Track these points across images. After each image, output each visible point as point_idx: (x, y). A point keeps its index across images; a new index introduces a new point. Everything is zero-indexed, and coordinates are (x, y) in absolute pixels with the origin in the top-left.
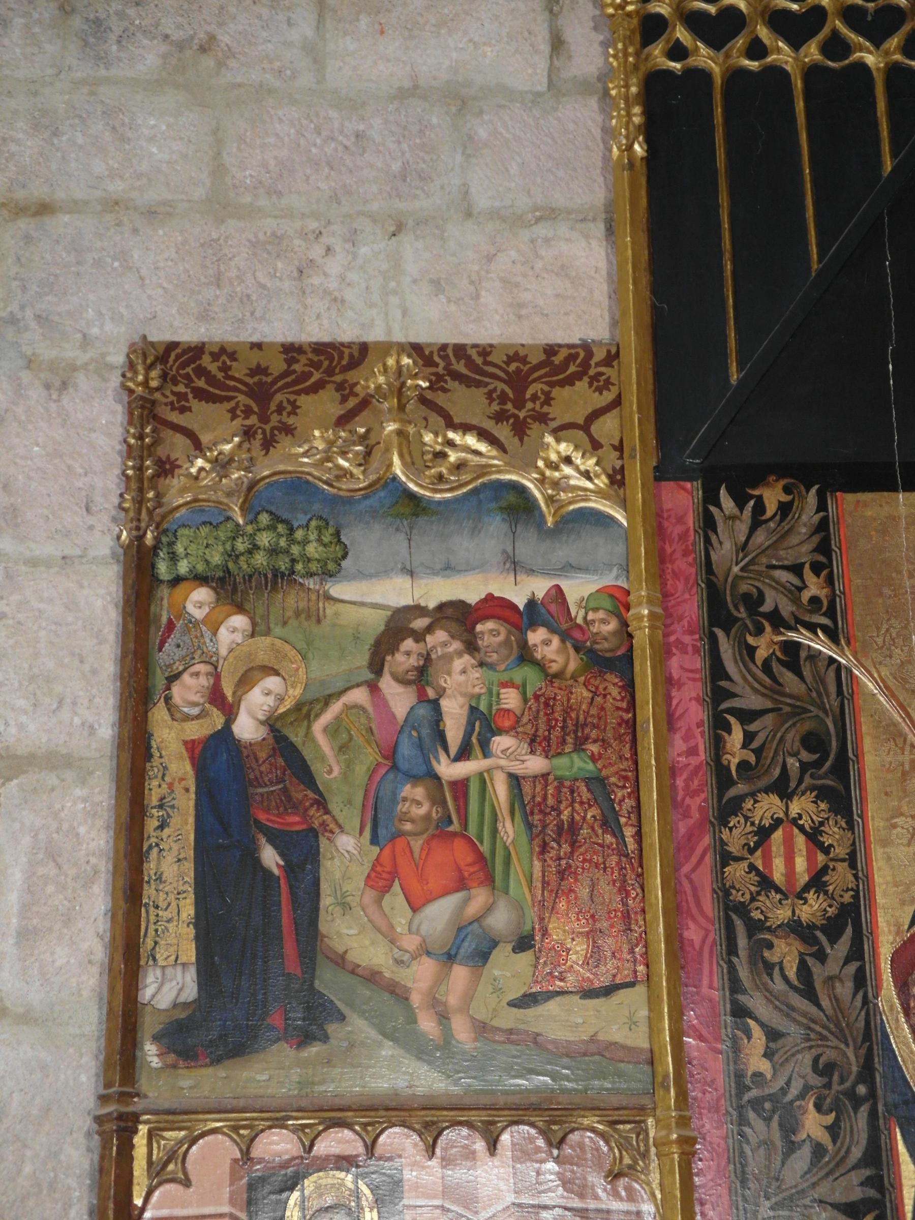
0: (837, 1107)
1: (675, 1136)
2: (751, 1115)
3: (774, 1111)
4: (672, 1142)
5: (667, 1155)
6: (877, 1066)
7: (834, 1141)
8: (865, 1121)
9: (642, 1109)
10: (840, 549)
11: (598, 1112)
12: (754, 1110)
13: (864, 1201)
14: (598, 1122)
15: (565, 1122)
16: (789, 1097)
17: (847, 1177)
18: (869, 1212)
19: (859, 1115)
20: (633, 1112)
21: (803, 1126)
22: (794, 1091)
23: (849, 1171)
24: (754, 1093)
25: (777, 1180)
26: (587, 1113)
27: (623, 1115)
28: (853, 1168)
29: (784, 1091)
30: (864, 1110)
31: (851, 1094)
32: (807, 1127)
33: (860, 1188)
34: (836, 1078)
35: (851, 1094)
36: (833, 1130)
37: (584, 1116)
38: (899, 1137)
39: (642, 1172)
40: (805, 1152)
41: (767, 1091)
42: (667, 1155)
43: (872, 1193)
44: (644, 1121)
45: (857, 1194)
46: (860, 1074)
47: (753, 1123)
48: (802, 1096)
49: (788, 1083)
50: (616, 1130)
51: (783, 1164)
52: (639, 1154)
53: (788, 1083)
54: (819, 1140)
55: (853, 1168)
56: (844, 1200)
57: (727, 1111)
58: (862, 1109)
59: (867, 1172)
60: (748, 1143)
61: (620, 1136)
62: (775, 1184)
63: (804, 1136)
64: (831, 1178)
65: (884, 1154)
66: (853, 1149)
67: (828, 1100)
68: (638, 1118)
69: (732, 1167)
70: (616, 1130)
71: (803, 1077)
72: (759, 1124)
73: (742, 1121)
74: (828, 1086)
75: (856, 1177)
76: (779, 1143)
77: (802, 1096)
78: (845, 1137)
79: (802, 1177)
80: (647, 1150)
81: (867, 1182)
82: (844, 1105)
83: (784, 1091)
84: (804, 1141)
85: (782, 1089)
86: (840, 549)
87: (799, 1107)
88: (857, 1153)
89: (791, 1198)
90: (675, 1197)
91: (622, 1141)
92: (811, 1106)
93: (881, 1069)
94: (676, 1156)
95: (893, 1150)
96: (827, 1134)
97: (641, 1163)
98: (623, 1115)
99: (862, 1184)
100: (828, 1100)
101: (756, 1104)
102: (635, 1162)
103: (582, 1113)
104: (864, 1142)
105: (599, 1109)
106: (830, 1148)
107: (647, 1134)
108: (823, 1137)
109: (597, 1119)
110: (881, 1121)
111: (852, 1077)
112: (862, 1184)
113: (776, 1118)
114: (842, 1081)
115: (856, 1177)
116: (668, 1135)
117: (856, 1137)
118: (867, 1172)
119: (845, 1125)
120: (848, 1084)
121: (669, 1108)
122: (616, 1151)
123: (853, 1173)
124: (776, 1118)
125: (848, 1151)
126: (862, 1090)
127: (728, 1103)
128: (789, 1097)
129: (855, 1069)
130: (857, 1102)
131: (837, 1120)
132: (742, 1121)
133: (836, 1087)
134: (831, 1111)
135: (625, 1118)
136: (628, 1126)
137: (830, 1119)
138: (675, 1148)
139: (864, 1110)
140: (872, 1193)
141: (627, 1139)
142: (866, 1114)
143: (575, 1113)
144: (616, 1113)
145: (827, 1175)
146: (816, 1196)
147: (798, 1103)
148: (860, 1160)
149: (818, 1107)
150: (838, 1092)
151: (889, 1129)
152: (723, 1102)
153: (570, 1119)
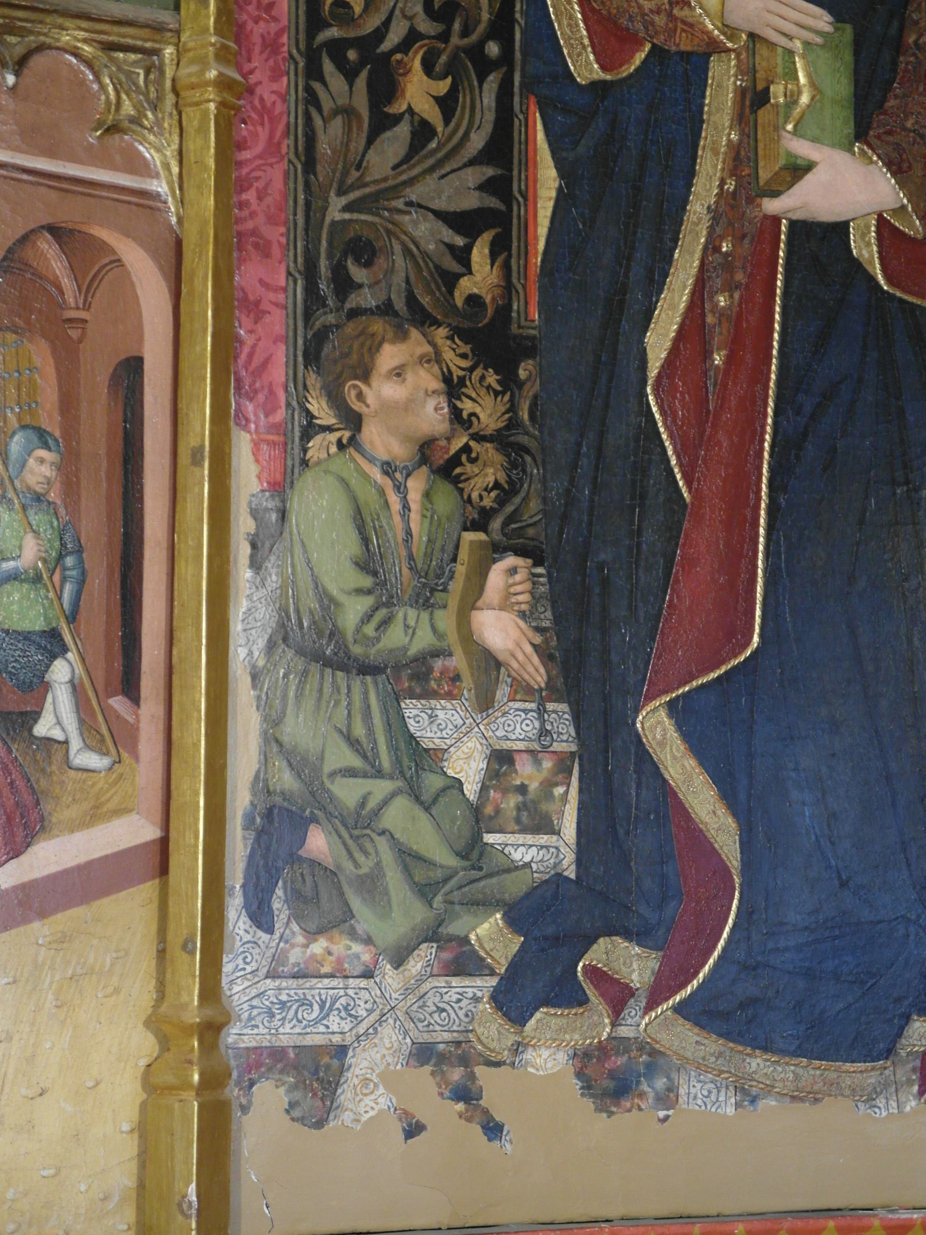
0: (451, 70)
1: (212, 74)
2: (328, 66)
3: (362, 64)
4: (207, 83)
5: (197, 104)
6: (518, 16)
7: (447, 121)
8: (493, 96)
9: (158, 29)
10: (524, 287)
11: (84, 24)
12: (333, 59)
13: (480, 213)
14: (85, 41)
15: (31, 32)
16: (386, 46)
17: (462, 173)
18: (487, 228)
19: (486, 86)
20: (145, 33)
21: (403, 92)
22: (394, 38)
23: (465, 166)
24: (333, 32)
25: (359, 167)
26: (68, 23)
27: (127, 36)
28: (471, 163)
29: (380, 34)
30: (492, 81)
31: (476, 53)
32: (408, 95)
33: (477, 194)
34: (457, 26)
35: (476, 53)
36: (447, 104)
37: (62, 28)
38: (541, 136)
39: (150, 130)
40: (403, 130)
41: (352, 34)
42: (197, 104)
43: (493, 202)
44: (156, 52)
45: (472, 201)
46: (492, 24)
47: (328, 78)
48: (405, 45)
49: (387, 23)
50: (112, 59)
51: (370, 142)
52: (148, 100)
53: (387, 23)
54: (425, 116)
55: (471, 163)
56: (452, 208)
57: (291, 56)
58: (491, 77)
59: (490, 172)
60: (319, 109)
61: (119, 69)
62: (355, 174)
63: (404, 107)
64: (436, 175)
65: (516, 147)
66: (473, 135)
67: (444, 58)
68: (148, 45)
69: (291, 141)
70: (112, 59)
71: (410, 18)
72: (335, 80)
73: (314, 72)
74: (444, 37)
75: (474, 176)
76: (365, 114)
77: (405, 45)
78: (463, 113)
79: (394, 168)
80: (160, 98)
81: (485, 187)
82: (466, 68)
83: (380, 34)
84: (403, 114)
85: (378, 29)
86: (524, 287)
87: (399, 62)
88: (477, 141)
89: (376, 196)
90: (206, 168)
91: (123, 78)
92: (417, 64)
93: (523, 22)
94: (212, 106)
95: (528, 140)
96: (437, 109)
97: (150, 114)
98: (127, 36)
99: (481, 188)
100: (444, 58)
101: (336, 49)
102: (141, 114)
103: (60, 20)
104: (488, 128)
105: (88, 18)
106: (440, 129)
107: (162, 72)
108: (430, 112)
109: (82, 34)
110: (517, 99)
111: (481, 28)
112: (481, 188)
113: (364, 74)
114: (465, 33)
115: (474, 176)
116: (202, 72)
117: (478, 117)
118: (490, 172)
119: (464, 99)
120: (474, 37)
121: (207, 30)
122: (110, 88)
123: (469, 170)
124: (364, 74)
125: (466, 136)
126: (493, 49)
127: (293, 42)
128: (386, 46)
129: (485, 16)
130: (484, 67)
131: (454, 89)
132: (314, 72)
133: (455, 40)
134: (445, 77)
135: (130, 41)
136: (133, 57)
137: (443, 87)
138: (211, 93)
139: (492, 81)
140: (493, 202)
141: (129, 74)
142: (495, 86)
143: (48, 19)
144: (116, 29)
145: (431, 170)
146: (414, 198)
147: (398, 56)
148: (480, 152)
149: (428, 68)
150: (458, 48)
151: (526, 114)
152: (284, 39)
153: (38, 28)
